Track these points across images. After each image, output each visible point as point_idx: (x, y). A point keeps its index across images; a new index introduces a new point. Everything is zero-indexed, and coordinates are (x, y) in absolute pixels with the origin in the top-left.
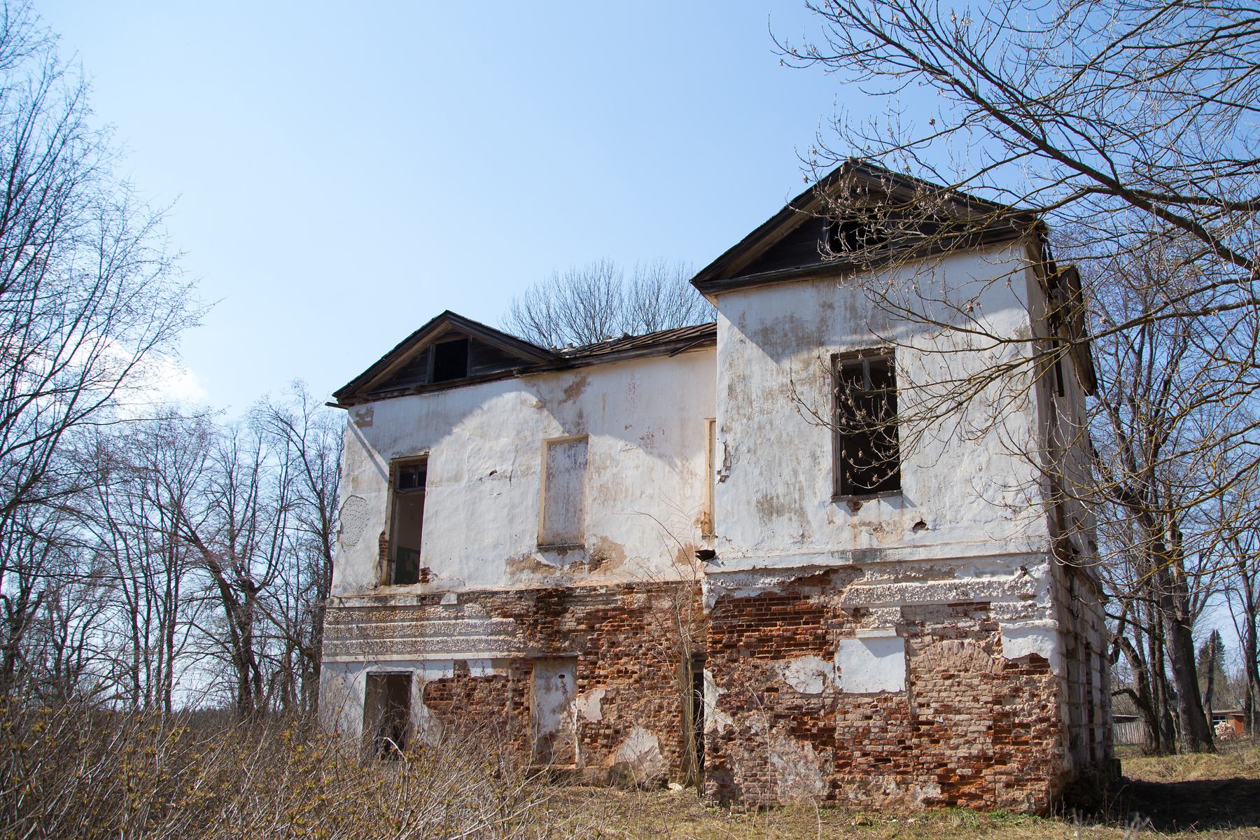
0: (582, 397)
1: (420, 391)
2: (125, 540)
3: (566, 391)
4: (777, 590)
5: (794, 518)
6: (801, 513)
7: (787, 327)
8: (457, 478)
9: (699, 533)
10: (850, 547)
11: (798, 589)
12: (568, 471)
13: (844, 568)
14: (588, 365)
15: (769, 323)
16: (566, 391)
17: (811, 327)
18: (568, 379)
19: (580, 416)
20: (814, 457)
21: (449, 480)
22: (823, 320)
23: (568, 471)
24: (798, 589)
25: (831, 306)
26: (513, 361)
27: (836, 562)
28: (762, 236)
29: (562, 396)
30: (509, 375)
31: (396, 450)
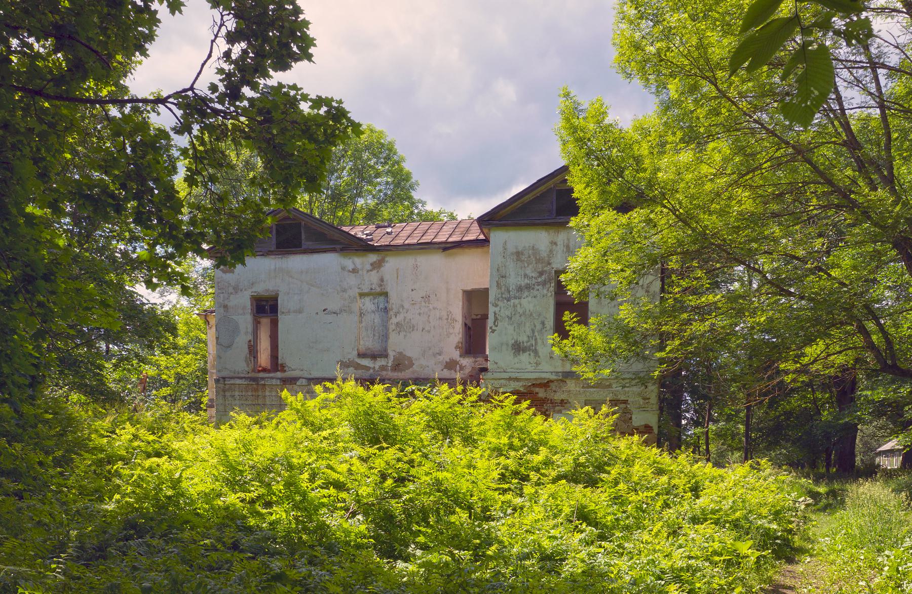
0: (382, 269)
1: (267, 253)
2: (707, 450)
3: (372, 265)
4: (522, 389)
5: (532, 354)
6: (536, 352)
7: (530, 252)
8: (300, 311)
9: (458, 353)
10: (560, 370)
11: (533, 389)
12: (373, 312)
13: (557, 380)
14: (390, 250)
15: (520, 249)
16: (372, 265)
17: (544, 254)
18: (373, 258)
19: (382, 280)
20: (543, 323)
21: (295, 312)
22: (551, 251)
23: (373, 312)
24: (533, 389)
25: (556, 244)
26: (333, 241)
27: (553, 377)
28: (519, 198)
29: (368, 267)
30: (333, 250)
31: (254, 290)
